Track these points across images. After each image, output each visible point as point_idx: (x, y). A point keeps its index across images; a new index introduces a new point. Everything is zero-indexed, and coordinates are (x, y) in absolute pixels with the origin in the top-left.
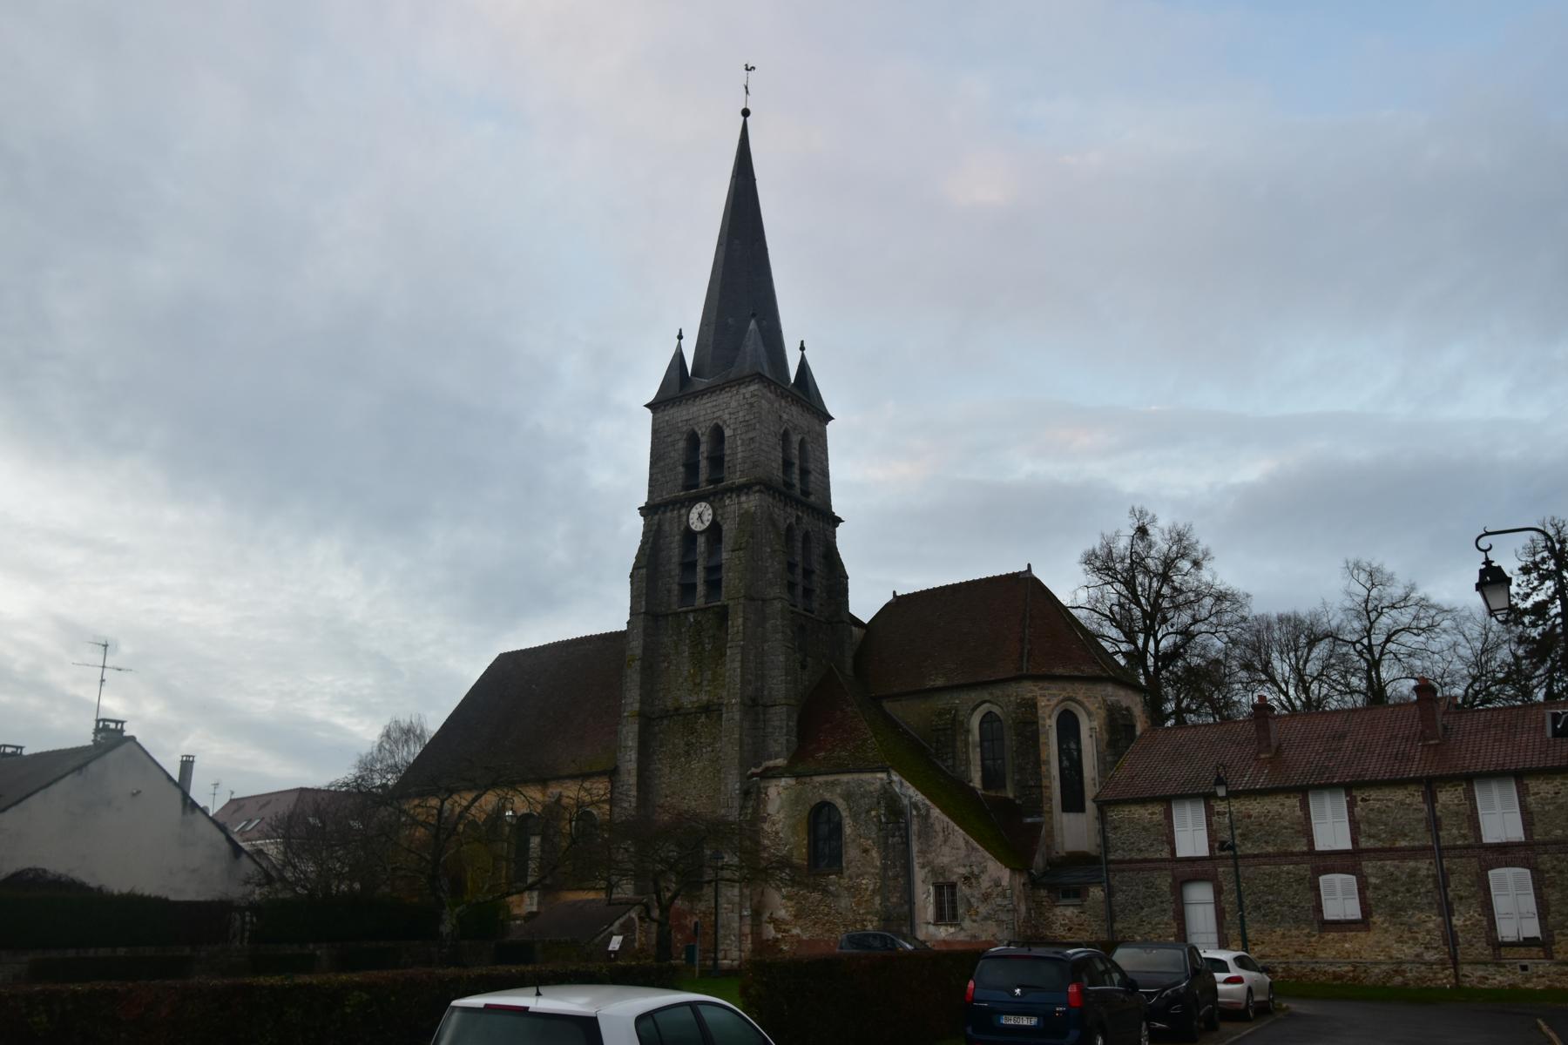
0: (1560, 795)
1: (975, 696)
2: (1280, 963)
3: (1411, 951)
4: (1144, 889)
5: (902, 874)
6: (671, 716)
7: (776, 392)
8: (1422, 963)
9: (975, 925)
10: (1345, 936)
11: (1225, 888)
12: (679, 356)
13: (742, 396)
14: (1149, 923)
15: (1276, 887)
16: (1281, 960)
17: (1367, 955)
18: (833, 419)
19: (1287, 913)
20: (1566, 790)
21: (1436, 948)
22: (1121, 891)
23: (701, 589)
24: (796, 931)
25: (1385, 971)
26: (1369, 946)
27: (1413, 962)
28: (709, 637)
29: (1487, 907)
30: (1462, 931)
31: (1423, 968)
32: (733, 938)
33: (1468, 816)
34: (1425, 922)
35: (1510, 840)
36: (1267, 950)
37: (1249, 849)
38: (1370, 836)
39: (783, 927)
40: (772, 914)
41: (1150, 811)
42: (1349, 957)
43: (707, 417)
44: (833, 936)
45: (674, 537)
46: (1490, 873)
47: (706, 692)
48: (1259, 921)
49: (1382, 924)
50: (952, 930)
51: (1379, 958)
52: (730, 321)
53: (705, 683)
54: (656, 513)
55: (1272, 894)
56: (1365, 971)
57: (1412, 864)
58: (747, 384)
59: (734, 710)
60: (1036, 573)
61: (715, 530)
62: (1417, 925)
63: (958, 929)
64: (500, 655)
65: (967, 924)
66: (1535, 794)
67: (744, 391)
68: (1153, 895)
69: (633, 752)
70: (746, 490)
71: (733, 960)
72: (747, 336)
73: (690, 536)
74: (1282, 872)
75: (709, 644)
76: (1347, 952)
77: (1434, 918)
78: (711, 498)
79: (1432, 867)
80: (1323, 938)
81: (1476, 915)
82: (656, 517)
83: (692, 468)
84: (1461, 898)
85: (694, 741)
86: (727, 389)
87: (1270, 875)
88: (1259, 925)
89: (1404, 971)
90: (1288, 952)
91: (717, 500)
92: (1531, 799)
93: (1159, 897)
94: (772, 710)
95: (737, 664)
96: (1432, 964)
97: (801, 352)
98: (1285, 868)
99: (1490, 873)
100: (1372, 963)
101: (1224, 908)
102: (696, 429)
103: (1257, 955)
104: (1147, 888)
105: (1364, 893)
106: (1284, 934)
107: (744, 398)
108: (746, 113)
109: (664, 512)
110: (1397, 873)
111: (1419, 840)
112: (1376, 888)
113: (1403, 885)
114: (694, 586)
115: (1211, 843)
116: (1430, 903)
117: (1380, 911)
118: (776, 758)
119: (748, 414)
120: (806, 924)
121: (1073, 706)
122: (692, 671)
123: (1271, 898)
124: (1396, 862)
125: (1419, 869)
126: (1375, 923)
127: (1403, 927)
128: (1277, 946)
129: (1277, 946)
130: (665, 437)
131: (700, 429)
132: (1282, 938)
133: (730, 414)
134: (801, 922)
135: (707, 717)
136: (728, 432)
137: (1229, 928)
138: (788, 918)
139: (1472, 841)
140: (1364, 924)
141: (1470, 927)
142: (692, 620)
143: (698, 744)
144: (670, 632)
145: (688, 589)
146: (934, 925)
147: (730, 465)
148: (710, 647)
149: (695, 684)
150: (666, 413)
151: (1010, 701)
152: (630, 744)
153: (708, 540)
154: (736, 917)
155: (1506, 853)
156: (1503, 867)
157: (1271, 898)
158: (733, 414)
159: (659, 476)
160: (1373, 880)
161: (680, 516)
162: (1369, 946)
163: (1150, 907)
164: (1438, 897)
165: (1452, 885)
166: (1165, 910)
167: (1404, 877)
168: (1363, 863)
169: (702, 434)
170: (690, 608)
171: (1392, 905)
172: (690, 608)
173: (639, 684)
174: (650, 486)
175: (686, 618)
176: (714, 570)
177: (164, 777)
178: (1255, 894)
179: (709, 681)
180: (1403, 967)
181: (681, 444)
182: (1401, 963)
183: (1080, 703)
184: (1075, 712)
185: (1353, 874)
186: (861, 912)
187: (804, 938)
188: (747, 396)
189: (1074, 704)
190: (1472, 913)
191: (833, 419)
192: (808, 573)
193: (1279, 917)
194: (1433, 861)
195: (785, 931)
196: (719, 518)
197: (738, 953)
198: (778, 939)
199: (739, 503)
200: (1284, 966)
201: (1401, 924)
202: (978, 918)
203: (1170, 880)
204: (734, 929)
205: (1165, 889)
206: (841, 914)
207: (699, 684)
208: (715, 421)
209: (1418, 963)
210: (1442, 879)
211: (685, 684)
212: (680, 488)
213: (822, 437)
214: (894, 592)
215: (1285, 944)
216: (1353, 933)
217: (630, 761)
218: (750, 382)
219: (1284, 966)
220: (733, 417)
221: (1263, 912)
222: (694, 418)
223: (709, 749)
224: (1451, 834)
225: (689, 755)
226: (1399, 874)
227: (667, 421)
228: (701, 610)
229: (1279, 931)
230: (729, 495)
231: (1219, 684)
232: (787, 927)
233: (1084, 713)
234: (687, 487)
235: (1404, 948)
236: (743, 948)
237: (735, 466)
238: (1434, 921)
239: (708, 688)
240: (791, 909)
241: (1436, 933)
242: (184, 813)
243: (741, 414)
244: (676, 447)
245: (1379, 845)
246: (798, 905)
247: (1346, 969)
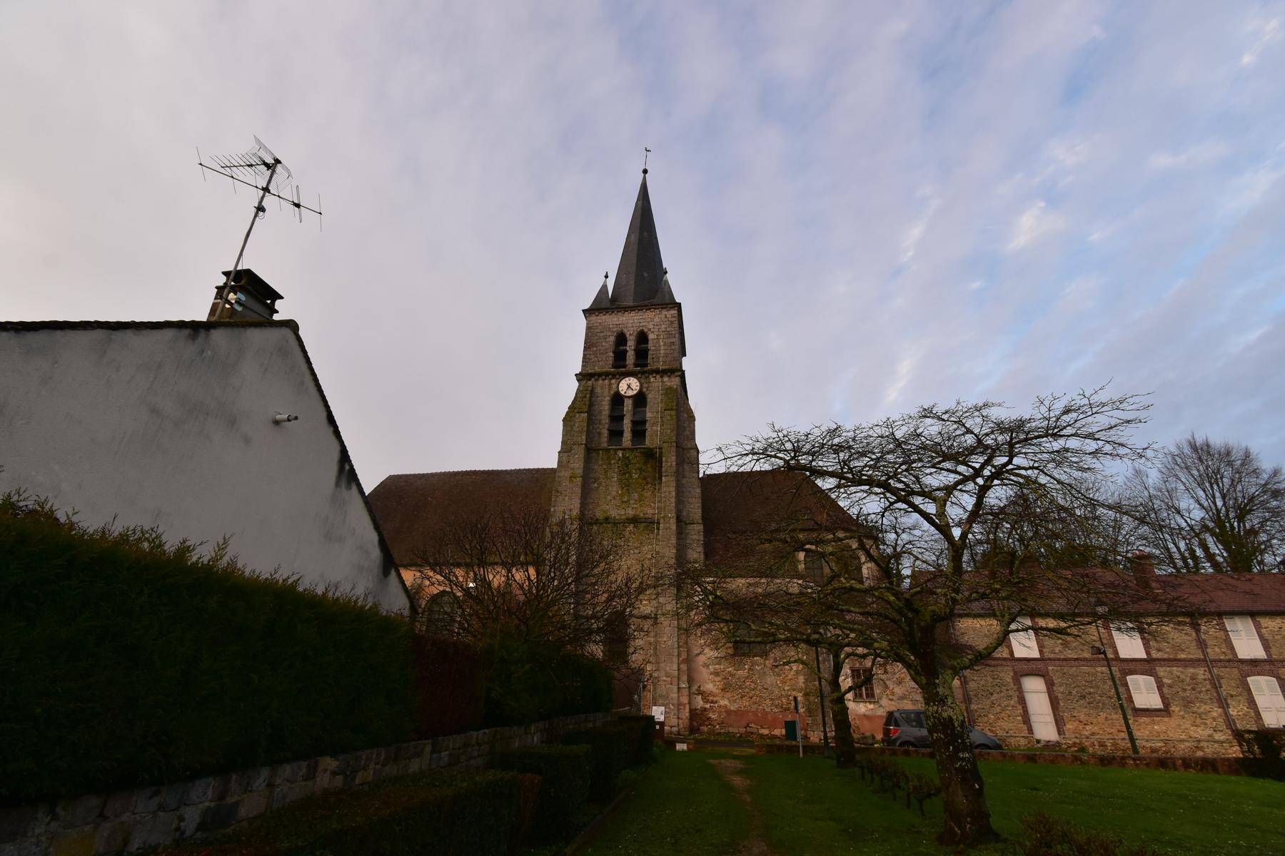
0: (1282, 629)
2: (1108, 739)
3: (1204, 732)
4: (992, 680)
5: (581, 659)
6: (601, 524)
8: (1214, 742)
9: (893, 703)
10: (1153, 720)
11: (1055, 681)
12: (604, 287)
14: (999, 705)
15: (1094, 682)
16: (1109, 736)
17: (1173, 735)
19: (1107, 702)
21: (1222, 731)
22: (973, 680)
23: (627, 435)
24: (724, 702)
25: (1189, 747)
26: (1173, 728)
27: (1208, 741)
28: (636, 469)
29: (1252, 703)
30: (1238, 719)
31: (1216, 745)
32: (672, 707)
33: (1225, 640)
34: (1210, 712)
35: (1258, 658)
36: (1096, 729)
37: (1070, 654)
38: (1159, 650)
39: (711, 698)
40: (699, 687)
42: (1159, 736)
43: (634, 325)
44: (761, 707)
45: (605, 397)
46: (1127, 677)
48: (1086, 707)
49: (1179, 712)
50: (871, 706)
51: (1182, 737)
52: (645, 274)
53: (632, 502)
54: (590, 380)
55: (1091, 687)
56: (1174, 747)
57: (1192, 670)
59: (671, 521)
61: (640, 399)
62: (1205, 714)
63: (877, 706)
64: (391, 478)
65: (884, 702)
66: (1265, 628)
68: (999, 684)
71: (671, 727)
73: (618, 399)
74: (1097, 672)
75: (635, 474)
76: (1157, 732)
77: (1216, 709)
78: (639, 375)
79: (1206, 673)
80: (1137, 721)
81: (1245, 708)
82: (590, 383)
84: (1232, 696)
86: (652, 310)
87: (1088, 674)
88: (1086, 710)
89: (1202, 747)
90: (1112, 731)
91: (643, 377)
92: (1264, 631)
93: (1004, 686)
94: (691, 527)
95: (673, 489)
96: (1222, 742)
98: (1099, 669)
99: (1127, 677)
100: (1178, 741)
101: (1057, 697)
102: (625, 330)
103: (1089, 732)
104: (994, 678)
105: (1162, 690)
106: (1106, 717)
107: (666, 317)
108: (645, 172)
109: (597, 380)
110: (1182, 676)
111: (1193, 654)
112: (1170, 686)
113: (1189, 685)
114: (621, 433)
115: (1267, 650)
116: (1211, 699)
117: (1176, 703)
120: (734, 696)
122: (620, 492)
123: (1092, 690)
124: (1180, 669)
125: (1197, 675)
126: (1173, 711)
127: (1194, 715)
128: (1103, 726)
129: (1103, 726)
131: (628, 331)
132: (1106, 720)
134: (728, 695)
137: (1064, 712)
138: (715, 690)
139: (1231, 656)
140: (1165, 711)
141: (1242, 716)
142: (621, 455)
144: (600, 462)
145: (616, 434)
146: (854, 701)
148: (636, 476)
149: (623, 502)
150: (598, 317)
154: (675, 689)
155: (1256, 666)
156: (1256, 675)
157: (1092, 690)
159: (592, 357)
160: (1166, 681)
161: (610, 385)
162: (1173, 728)
163: (998, 693)
164: (1215, 694)
165: (1224, 687)
166: (1011, 696)
167: (1188, 679)
168: (1157, 668)
170: (618, 447)
171: (1183, 698)
172: (618, 447)
173: (580, 495)
174: (583, 362)
177: (324, 414)
178: (1079, 686)
179: (636, 501)
180: (1202, 744)
181: (612, 339)
182: (1199, 741)
185: (1151, 676)
186: (786, 688)
187: (732, 708)
190: (1241, 706)
193: (1100, 705)
194: (1206, 669)
195: (712, 702)
196: (644, 390)
197: (677, 720)
198: (705, 708)
199: (663, 382)
200: (1111, 741)
201: (1193, 713)
202: (894, 698)
203: (1012, 674)
204: (672, 699)
205: (1009, 681)
206: (767, 689)
209: (1212, 741)
210: (1215, 684)
212: (610, 366)
215: (1109, 725)
216: (1158, 718)
218: (671, 308)
219: (1111, 741)
221: (1088, 700)
222: (623, 324)
223: (636, 551)
224: (1214, 652)
226: (1184, 677)
228: (629, 449)
229: (1103, 715)
230: (655, 375)
232: (715, 699)
235: (1198, 730)
236: (681, 716)
238: (1216, 712)
240: (718, 683)
241: (1220, 720)
242: (338, 484)
244: (607, 340)
245: (1166, 656)
246: (725, 681)
247: (1159, 745)
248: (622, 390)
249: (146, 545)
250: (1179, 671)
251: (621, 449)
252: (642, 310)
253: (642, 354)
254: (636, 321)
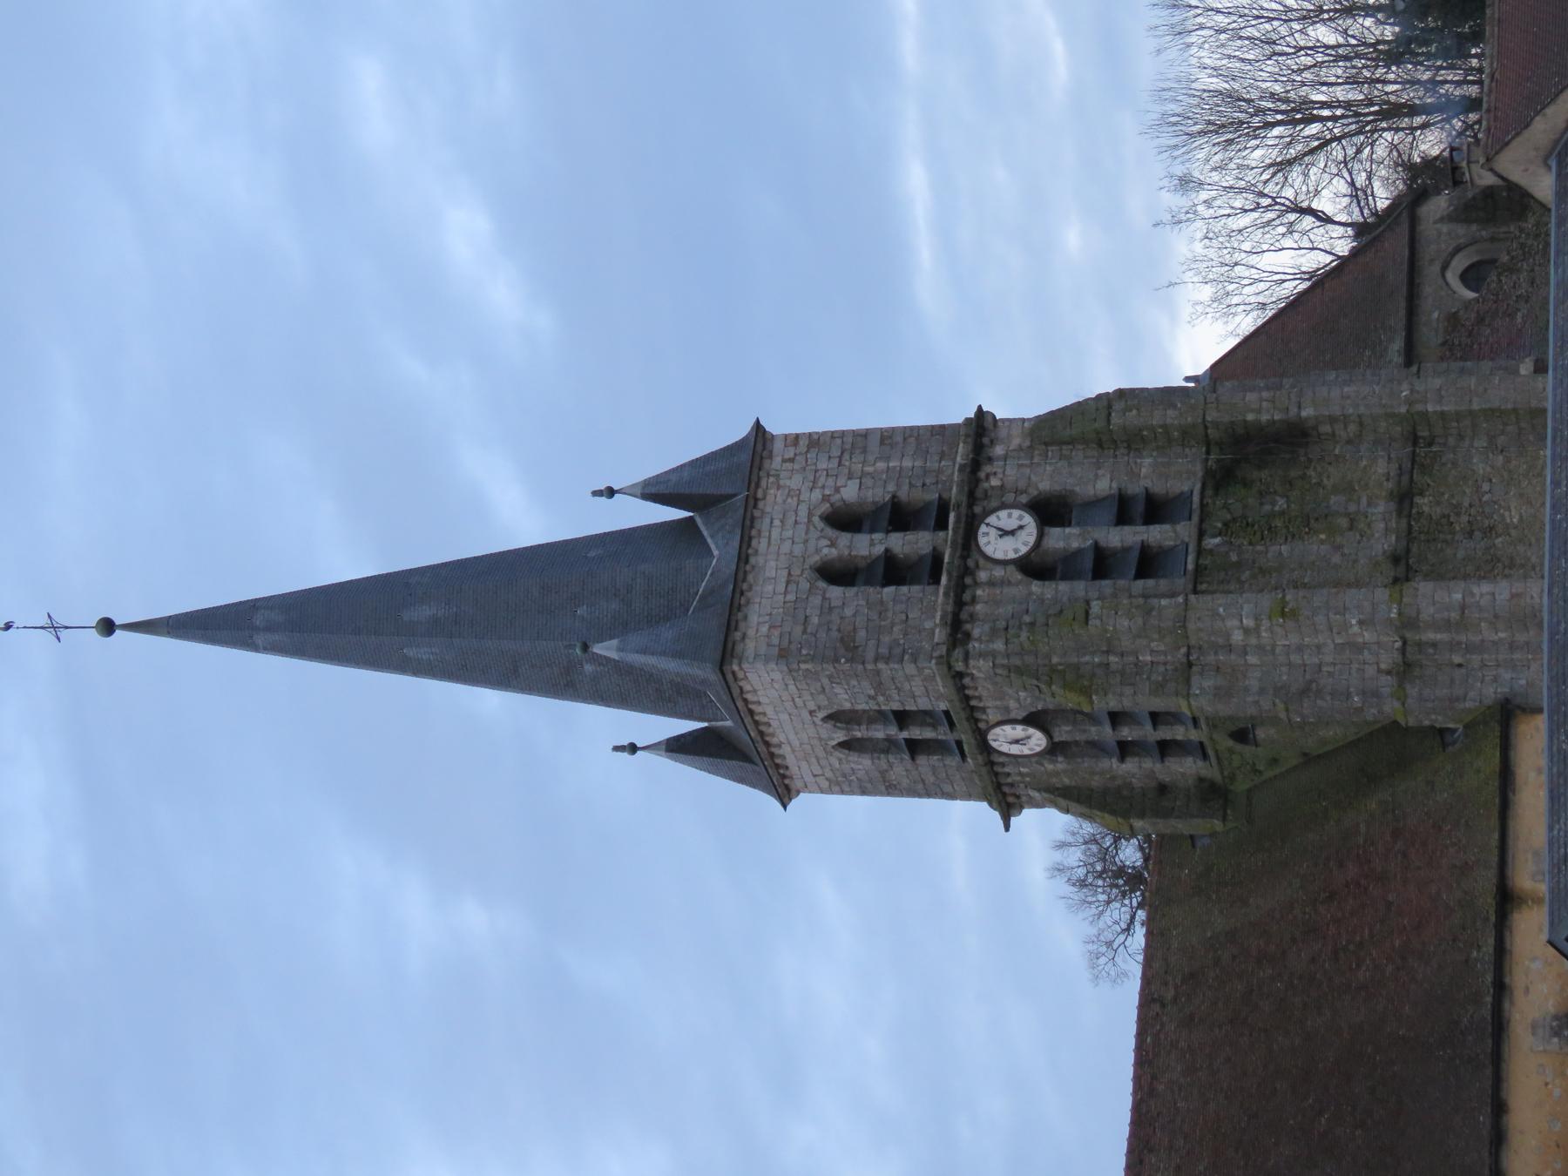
1: (1428, 290)
28: (1262, 504)
47: (1369, 504)
53: (1352, 508)
58: (765, 453)
67: (778, 460)
69: (1476, 590)
70: (986, 440)
85: (1465, 518)
107: (792, 460)
108: (107, 627)
130: (804, 632)
135: (1421, 494)
142: (1217, 540)
143: (1473, 511)
149: (1351, 528)
151: (1449, 234)
152: (1458, 596)
175: (1211, 552)
176: (1124, 510)
207: (1352, 521)
208: (816, 519)
211: (1346, 551)
217: (1493, 594)
220: (822, 480)
225: (1491, 528)
231: (1445, 53)
237: (925, 471)
239: (1364, 500)
243: (823, 464)
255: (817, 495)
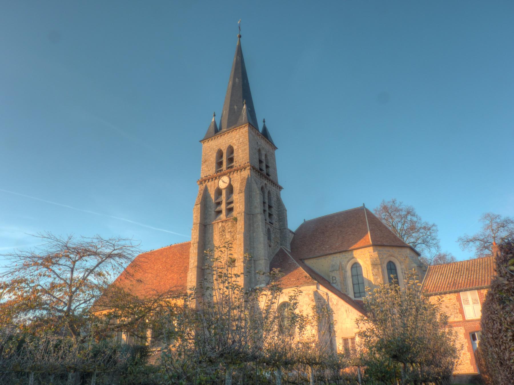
7: (255, 132)
13: (241, 133)
18: (277, 148)
20: (229, 381)
41: (448, 298)
60: (367, 206)
61: (230, 189)
67: (242, 130)
72: (243, 111)
73: (219, 192)
83: (220, 164)
86: (235, 131)
97: (263, 123)
107: (242, 133)
118: (260, 284)
119: (173, 269)
121: (393, 259)
125: (53, 344)
131: (223, 148)
133: (236, 140)
136: (235, 147)
147: (236, 160)
153: (226, 192)
158: (237, 140)
169: (224, 150)
181: (215, 155)
183: (397, 258)
184: (394, 262)
188: (243, 132)
189: (393, 258)
191: (277, 148)
192: (270, 207)
213: (273, 155)
214: (304, 220)
227: (209, 147)
233: (397, 261)
234: (217, 172)
248: (220, 185)
249: (56, 335)
250: (67, 326)
251: (221, 222)
252: (229, 132)
253: (231, 160)
254: (227, 140)
255: (235, 141)
